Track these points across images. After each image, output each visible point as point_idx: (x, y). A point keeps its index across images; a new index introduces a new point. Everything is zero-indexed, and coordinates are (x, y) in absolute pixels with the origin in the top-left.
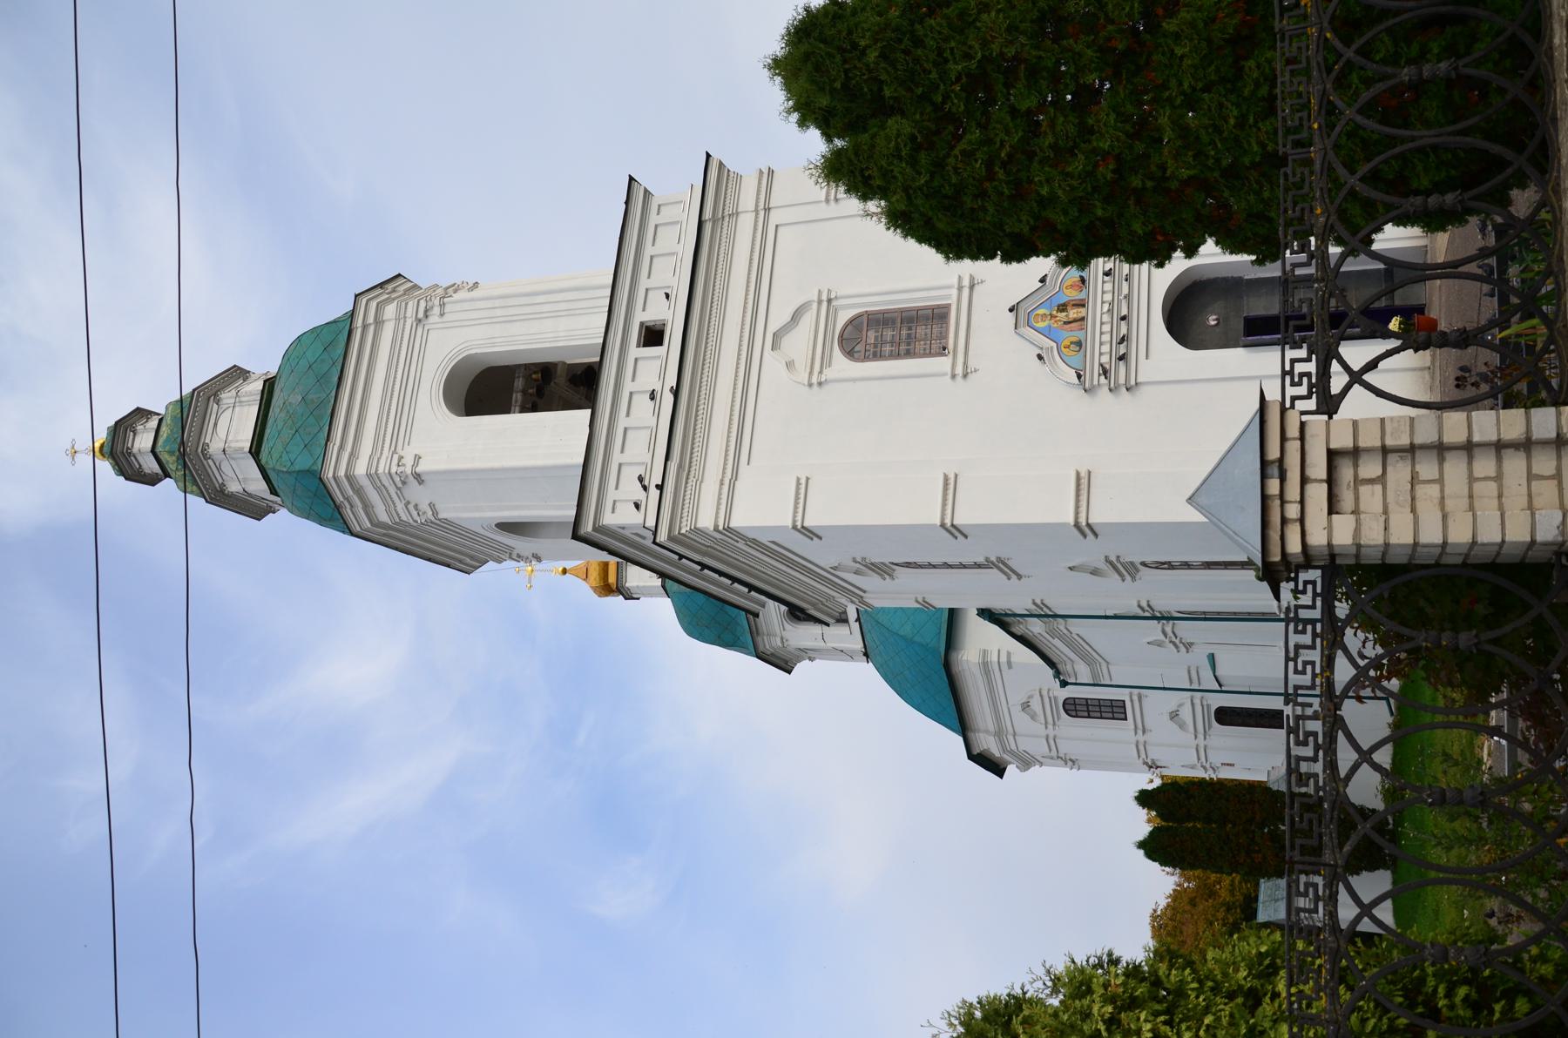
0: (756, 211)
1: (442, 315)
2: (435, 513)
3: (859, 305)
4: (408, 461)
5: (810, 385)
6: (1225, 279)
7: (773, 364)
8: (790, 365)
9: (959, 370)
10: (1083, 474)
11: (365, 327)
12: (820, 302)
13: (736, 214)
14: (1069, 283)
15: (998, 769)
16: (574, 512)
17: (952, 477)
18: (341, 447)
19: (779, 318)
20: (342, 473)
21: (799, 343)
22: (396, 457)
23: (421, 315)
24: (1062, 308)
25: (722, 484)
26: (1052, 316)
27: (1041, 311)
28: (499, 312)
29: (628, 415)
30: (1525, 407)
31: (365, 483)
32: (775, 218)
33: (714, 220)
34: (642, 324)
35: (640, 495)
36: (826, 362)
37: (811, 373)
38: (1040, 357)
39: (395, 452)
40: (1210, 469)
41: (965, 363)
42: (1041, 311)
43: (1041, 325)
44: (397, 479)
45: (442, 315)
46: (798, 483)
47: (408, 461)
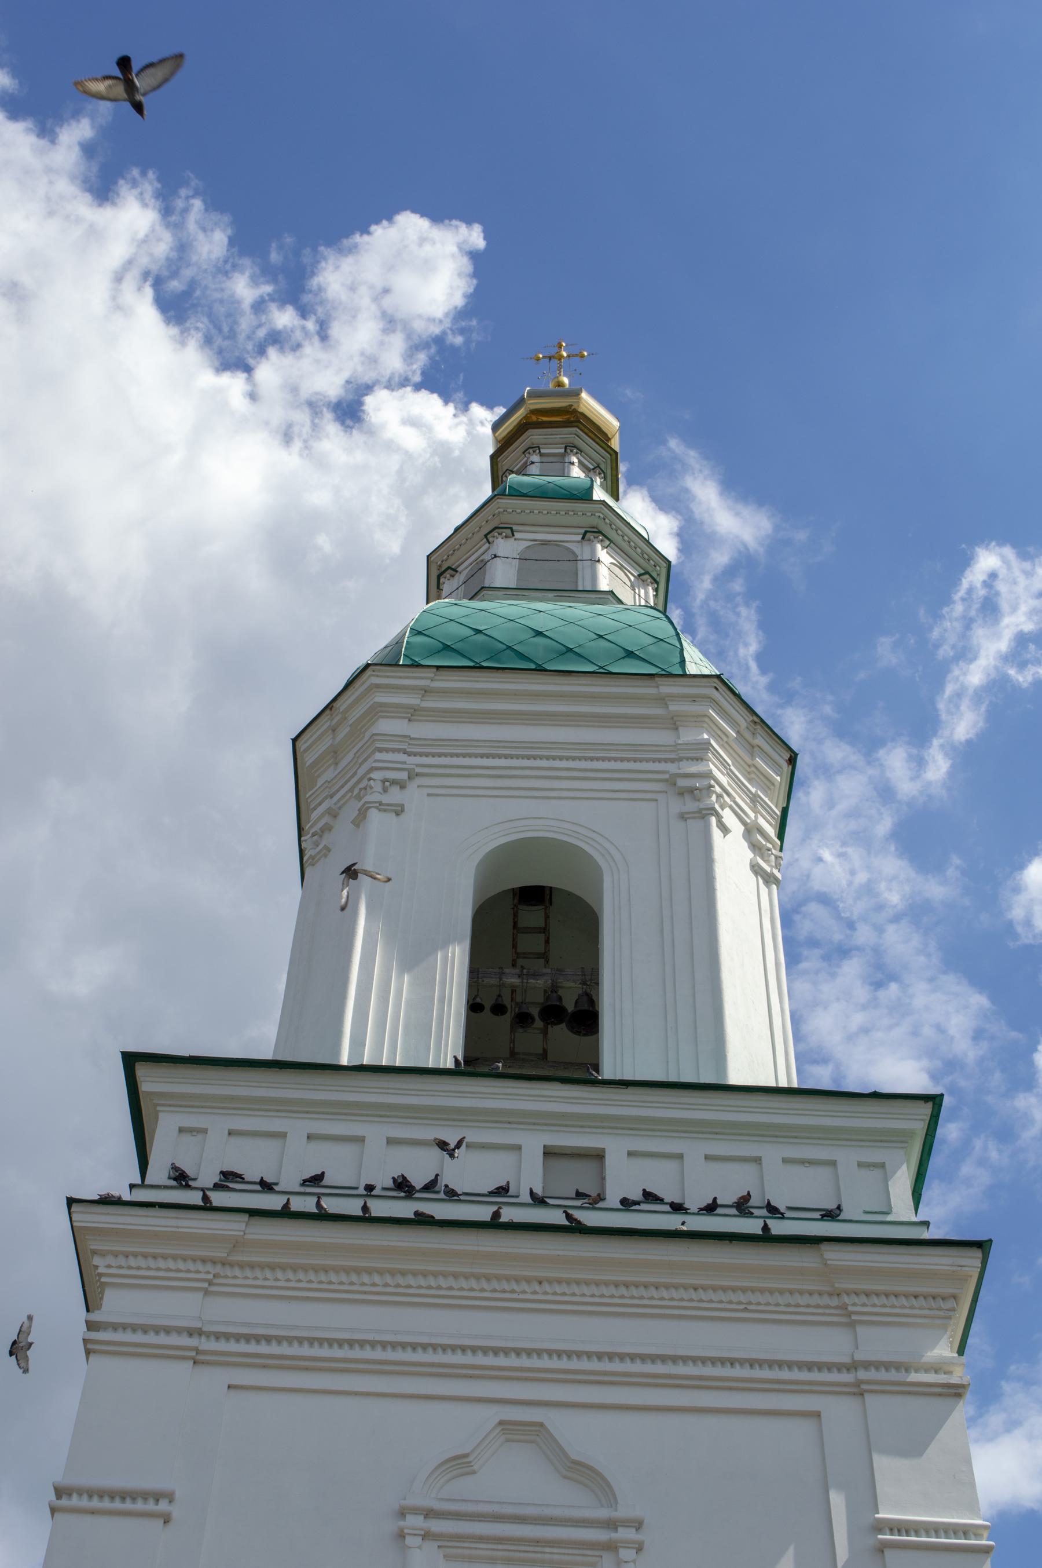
0: (852, 1366)
1: (683, 817)
4: (394, 796)
5: (402, 1513)
6: (598, 949)
7: (463, 1426)
8: (459, 1464)
12: (612, 1524)
15: (11, 1354)
19: (578, 1434)
20: (381, 698)
22: (404, 776)
23: (682, 783)
25: (191, 1332)
32: (838, 1411)
34: (603, 1150)
35: (613, 1199)
37: (429, 1514)
40: (670, 588)
45: (683, 817)
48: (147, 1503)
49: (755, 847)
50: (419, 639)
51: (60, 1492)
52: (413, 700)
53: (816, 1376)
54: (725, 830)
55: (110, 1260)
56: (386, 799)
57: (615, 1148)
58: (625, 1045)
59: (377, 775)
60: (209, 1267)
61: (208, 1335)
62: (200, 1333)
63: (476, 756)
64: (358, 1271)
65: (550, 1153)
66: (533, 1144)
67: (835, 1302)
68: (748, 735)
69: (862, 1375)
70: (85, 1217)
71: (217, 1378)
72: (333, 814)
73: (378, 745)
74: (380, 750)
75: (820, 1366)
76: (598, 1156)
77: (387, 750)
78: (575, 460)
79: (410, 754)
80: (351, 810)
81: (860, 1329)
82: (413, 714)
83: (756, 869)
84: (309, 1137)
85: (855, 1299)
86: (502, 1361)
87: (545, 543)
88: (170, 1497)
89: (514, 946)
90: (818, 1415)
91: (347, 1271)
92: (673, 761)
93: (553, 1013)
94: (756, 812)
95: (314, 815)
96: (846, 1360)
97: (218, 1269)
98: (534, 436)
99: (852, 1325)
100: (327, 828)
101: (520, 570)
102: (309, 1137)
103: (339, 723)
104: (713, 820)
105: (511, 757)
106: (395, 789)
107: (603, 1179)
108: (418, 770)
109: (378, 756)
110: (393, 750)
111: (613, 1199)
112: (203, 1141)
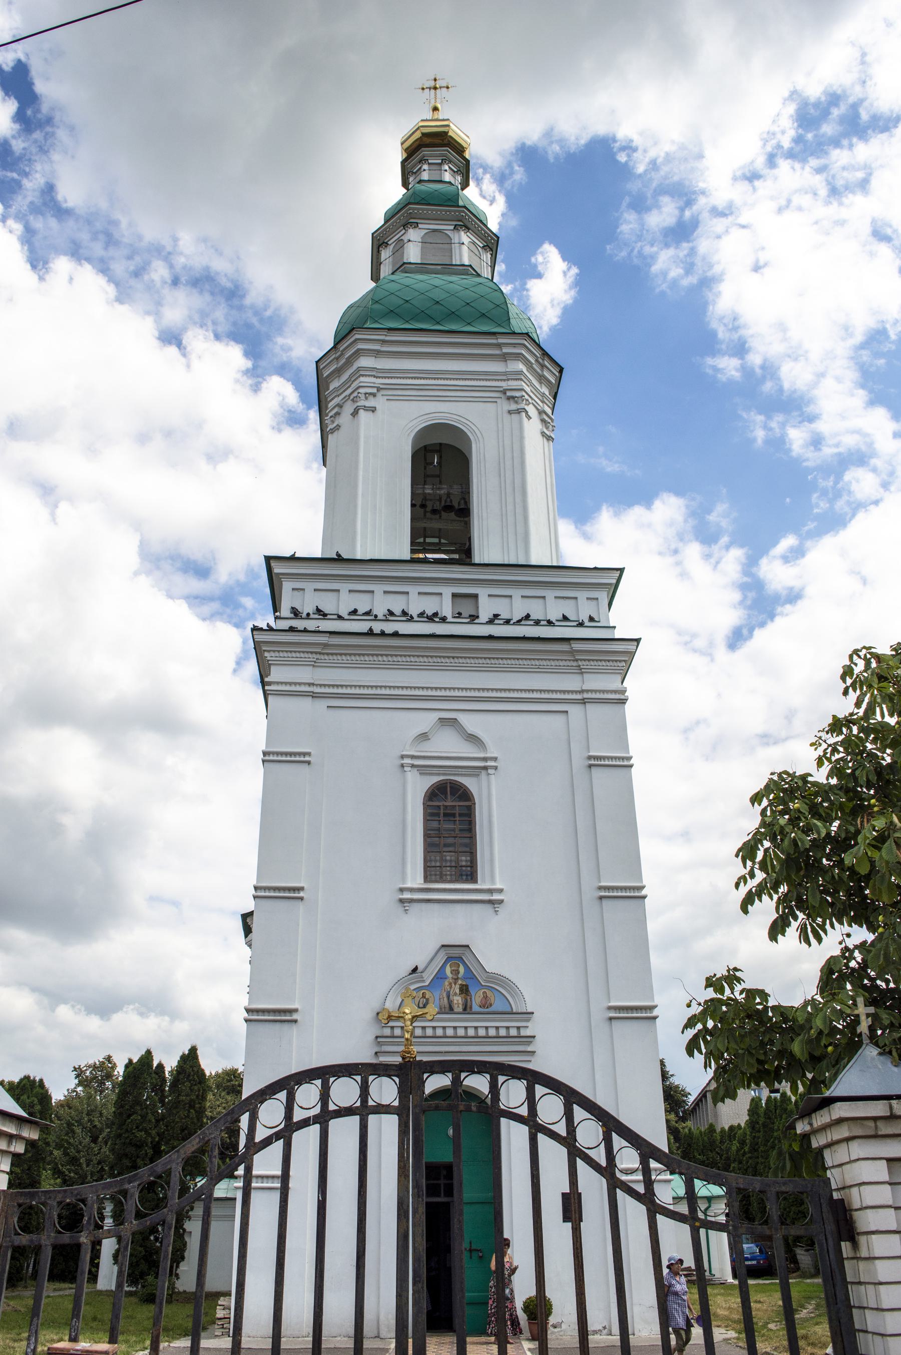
0: (582, 691)
1: (510, 412)
2: (332, 431)
3: (480, 795)
4: (371, 402)
7: (425, 721)
8: (424, 737)
9: (407, 895)
10: (295, 1016)
11: (499, 346)
12: (485, 759)
13: (581, 672)
14: (489, 994)
16: (359, 558)
17: (301, 894)
18: (384, 342)
19: (471, 723)
20: (361, 346)
21: (447, 745)
22: (374, 390)
23: (509, 394)
24: (464, 990)
25: (310, 684)
26: (456, 979)
27: (462, 969)
28: (508, 463)
29: (556, 597)
30: (825, 1169)
31: (355, 367)
32: (575, 711)
33: (572, 652)
35: (484, 616)
36: (423, 770)
37: (413, 757)
38: (415, 970)
39: (379, 389)
41: (412, 901)
42: (462, 969)
43: (448, 970)
44: (355, 394)
46: (304, 754)
47: (371, 402)
48: (300, 759)
49: (543, 421)
50: (377, 306)
51: (265, 754)
52: (376, 347)
53: (567, 696)
54: (529, 418)
55: (272, 654)
56: (367, 404)
57: (483, 593)
58: (488, 547)
59: (362, 390)
60: (314, 656)
61: (317, 685)
62: (313, 684)
63: (409, 378)
64: (377, 655)
65: (455, 596)
66: (447, 591)
67: (575, 664)
68: (540, 360)
69: (586, 695)
70: (260, 637)
71: (323, 704)
72: (340, 406)
73: (362, 373)
74: (363, 375)
75: (569, 692)
76: (476, 596)
77: (366, 375)
78: (446, 167)
79: (377, 377)
80: (349, 408)
81: (585, 675)
82: (377, 354)
83: (543, 434)
84: (350, 591)
85: (584, 663)
86: (438, 693)
87: (435, 231)
88: (309, 754)
89: (425, 459)
90: (567, 712)
91: (373, 655)
92: (504, 380)
93: (448, 508)
94: (543, 402)
95: (331, 405)
96: (579, 689)
97: (318, 656)
98: (426, 152)
99: (582, 673)
100: (338, 414)
101: (422, 248)
102: (350, 591)
103: (340, 356)
104: (524, 414)
105: (427, 378)
106: (371, 398)
107: (478, 608)
108: (381, 386)
109: (362, 379)
110: (369, 376)
111: (484, 616)
112: (301, 596)
